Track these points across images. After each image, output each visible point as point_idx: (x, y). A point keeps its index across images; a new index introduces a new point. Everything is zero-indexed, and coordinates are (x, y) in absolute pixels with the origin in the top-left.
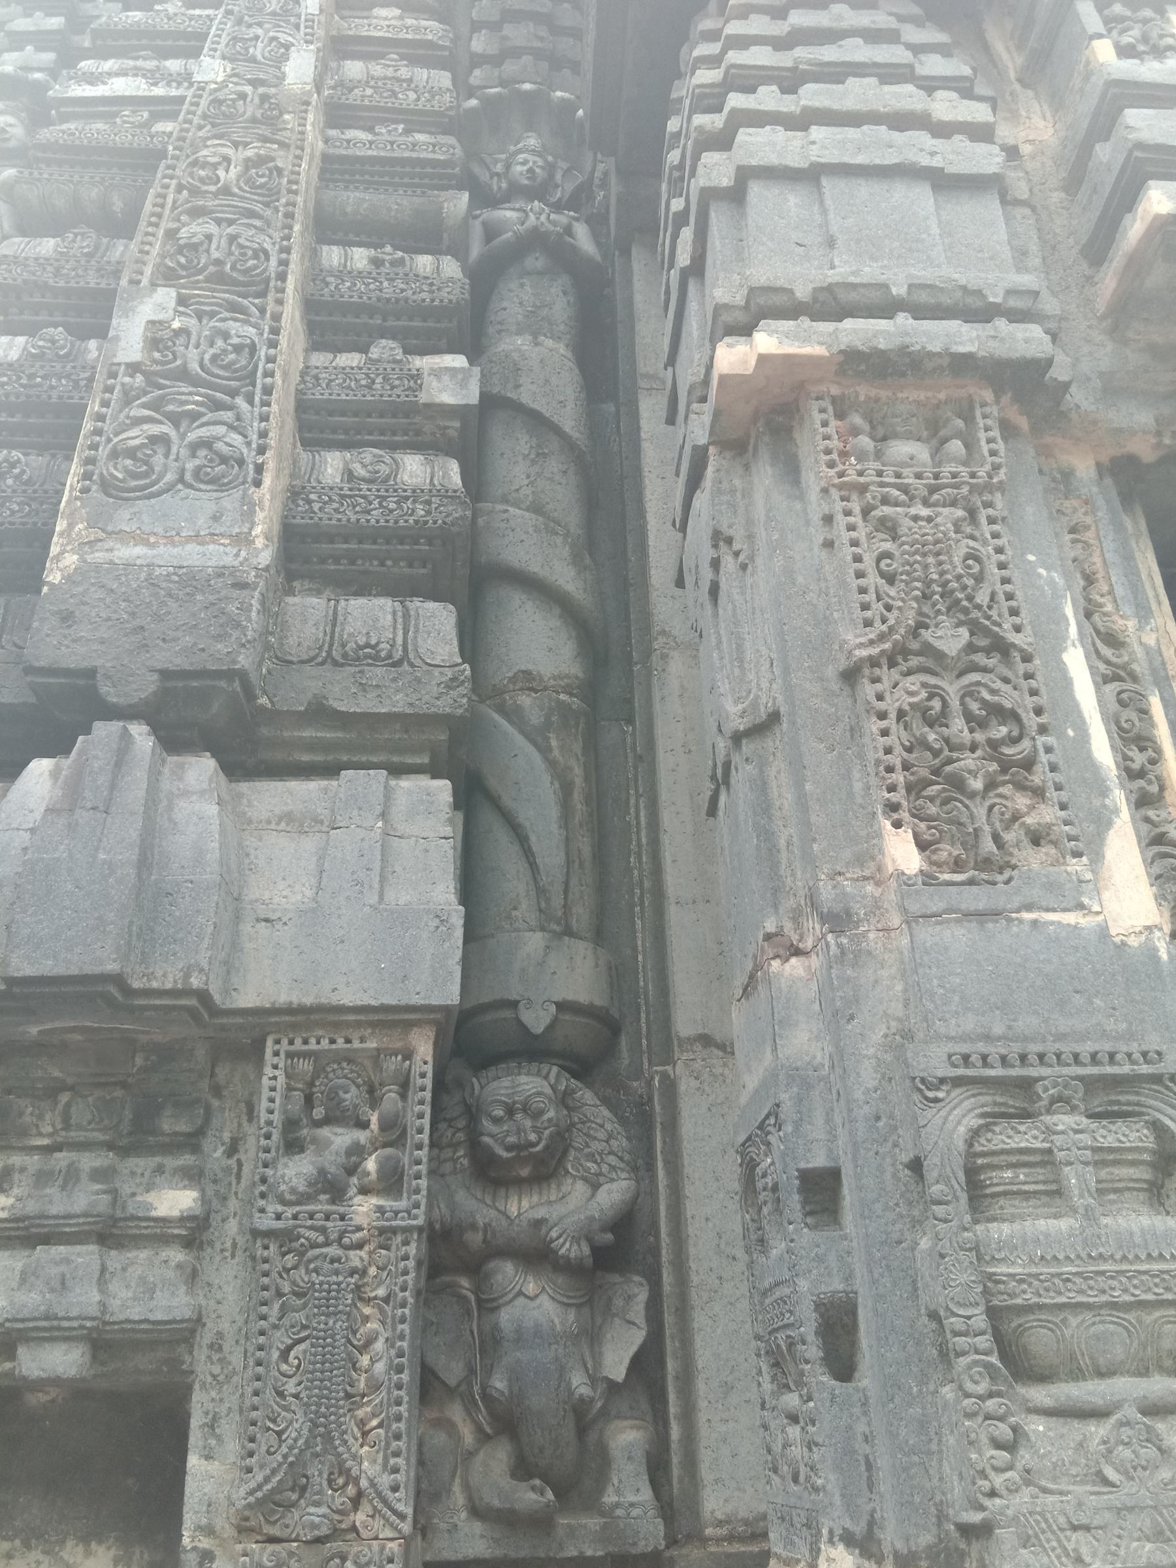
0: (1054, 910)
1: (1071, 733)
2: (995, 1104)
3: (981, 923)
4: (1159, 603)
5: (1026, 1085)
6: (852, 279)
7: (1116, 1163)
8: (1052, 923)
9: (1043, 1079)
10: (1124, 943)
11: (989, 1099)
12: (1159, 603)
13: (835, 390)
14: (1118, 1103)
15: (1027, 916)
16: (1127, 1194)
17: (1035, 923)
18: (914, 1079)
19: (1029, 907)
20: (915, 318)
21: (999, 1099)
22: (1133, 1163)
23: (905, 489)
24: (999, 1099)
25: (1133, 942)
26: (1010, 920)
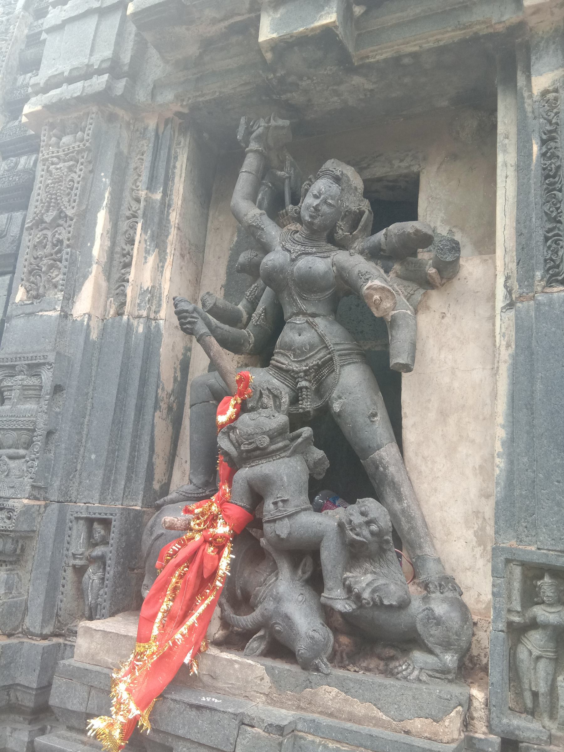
0: (47, 311)
1: (89, 244)
2: (9, 373)
3: (28, 317)
4: (181, 177)
5: (13, 367)
6: (56, 73)
7: (27, 390)
8: (45, 315)
9: (17, 365)
10: (76, 320)
11: (7, 371)
12: (181, 177)
13: (51, 120)
14: (36, 372)
15: (40, 313)
16: (33, 399)
17: (41, 315)
18: (237, 367)
19: (41, 311)
20: (44, 94)
21: (10, 371)
22: (35, 390)
23: (58, 157)
24: (10, 371)
25: (79, 319)
26: (36, 315)
